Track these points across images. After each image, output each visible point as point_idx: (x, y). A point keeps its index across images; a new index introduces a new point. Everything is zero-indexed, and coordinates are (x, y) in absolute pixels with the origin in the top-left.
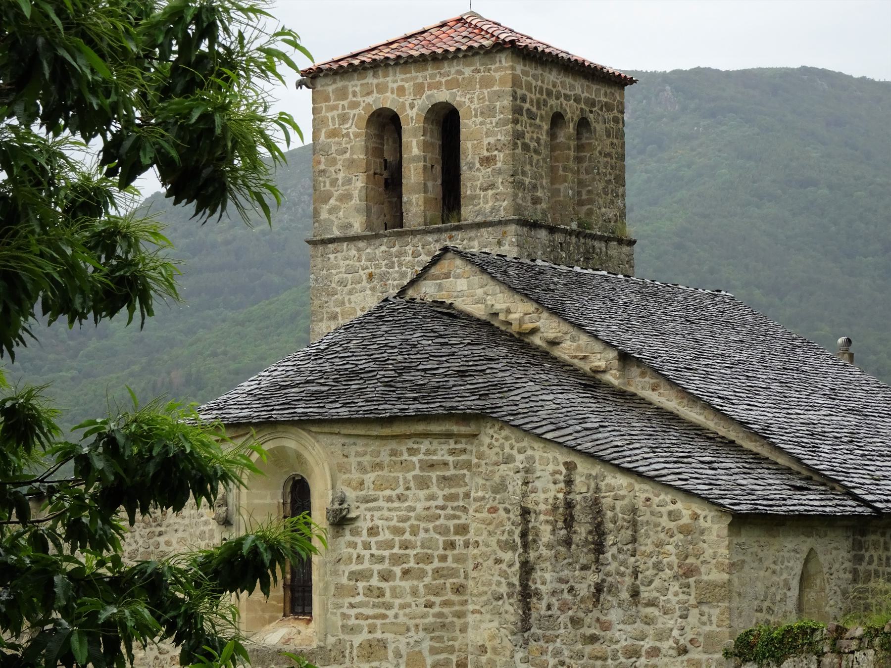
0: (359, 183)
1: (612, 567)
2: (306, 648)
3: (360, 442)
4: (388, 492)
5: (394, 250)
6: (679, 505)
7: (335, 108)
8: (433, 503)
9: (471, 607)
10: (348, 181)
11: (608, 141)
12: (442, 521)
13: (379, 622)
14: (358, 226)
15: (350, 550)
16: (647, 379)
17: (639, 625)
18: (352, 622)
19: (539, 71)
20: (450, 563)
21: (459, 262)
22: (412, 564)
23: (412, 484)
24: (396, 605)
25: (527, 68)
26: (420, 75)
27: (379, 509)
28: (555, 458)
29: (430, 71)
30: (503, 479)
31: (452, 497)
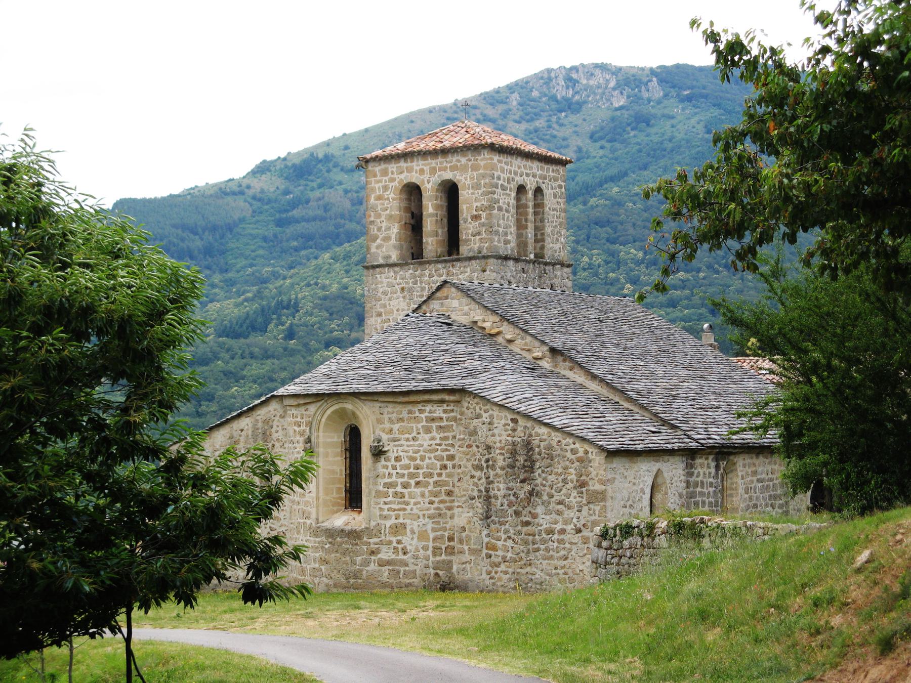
0: (395, 230)
1: (539, 481)
2: (358, 528)
3: (390, 405)
4: (407, 436)
5: (417, 273)
6: (577, 445)
7: (380, 181)
8: (433, 442)
9: (456, 504)
10: (388, 229)
11: (555, 201)
12: (439, 453)
13: (401, 513)
14: (394, 257)
15: (385, 470)
16: (567, 363)
17: (554, 516)
18: (386, 513)
19: (509, 159)
20: (444, 478)
21: (453, 290)
22: (421, 478)
23: (421, 431)
24: (412, 503)
25: (501, 158)
26: (433, 161)
27: (401, 445)
28: (506, 416)
29: (440, 159)
30: (475, 427)
31: (446, 438)
